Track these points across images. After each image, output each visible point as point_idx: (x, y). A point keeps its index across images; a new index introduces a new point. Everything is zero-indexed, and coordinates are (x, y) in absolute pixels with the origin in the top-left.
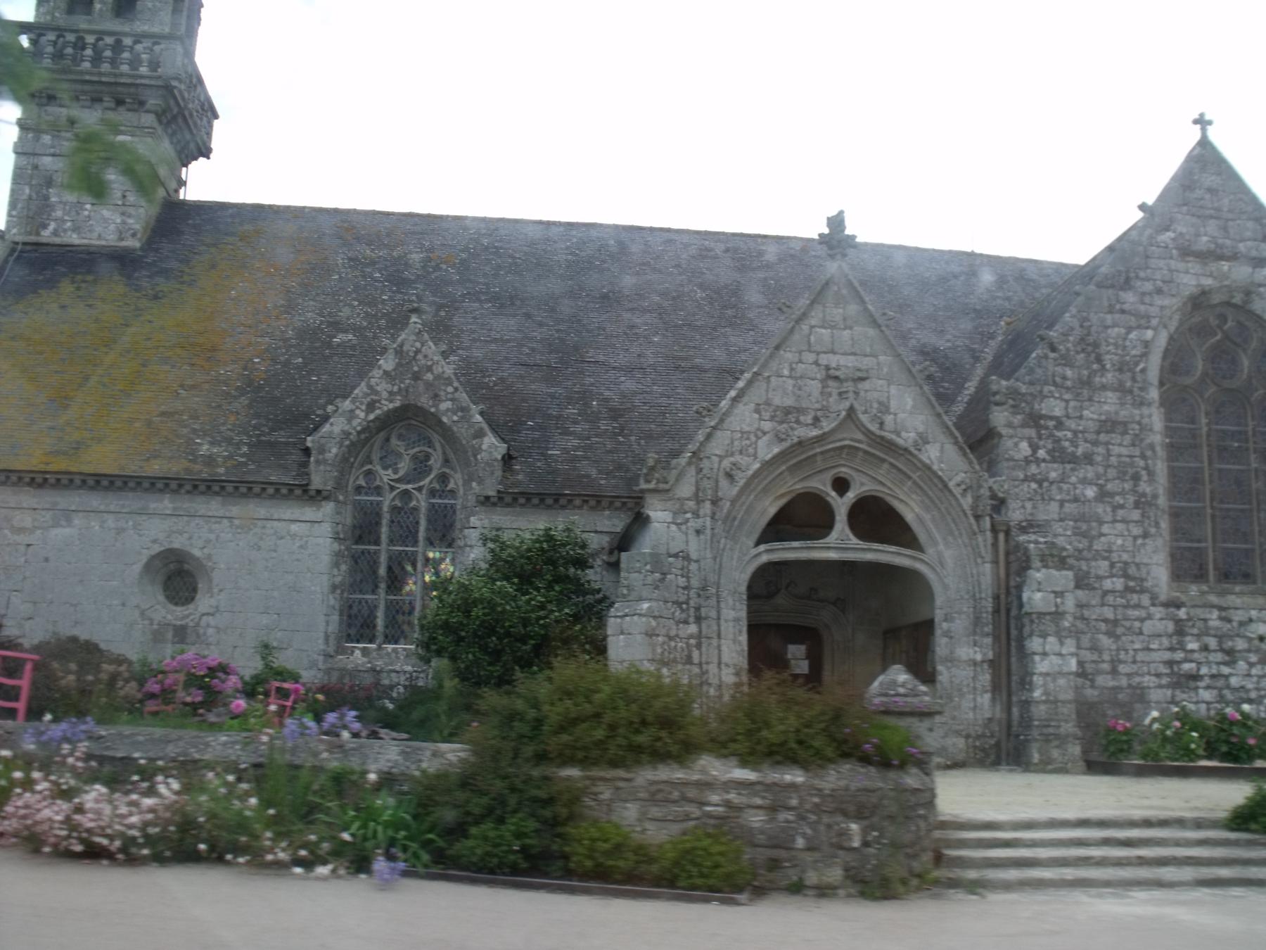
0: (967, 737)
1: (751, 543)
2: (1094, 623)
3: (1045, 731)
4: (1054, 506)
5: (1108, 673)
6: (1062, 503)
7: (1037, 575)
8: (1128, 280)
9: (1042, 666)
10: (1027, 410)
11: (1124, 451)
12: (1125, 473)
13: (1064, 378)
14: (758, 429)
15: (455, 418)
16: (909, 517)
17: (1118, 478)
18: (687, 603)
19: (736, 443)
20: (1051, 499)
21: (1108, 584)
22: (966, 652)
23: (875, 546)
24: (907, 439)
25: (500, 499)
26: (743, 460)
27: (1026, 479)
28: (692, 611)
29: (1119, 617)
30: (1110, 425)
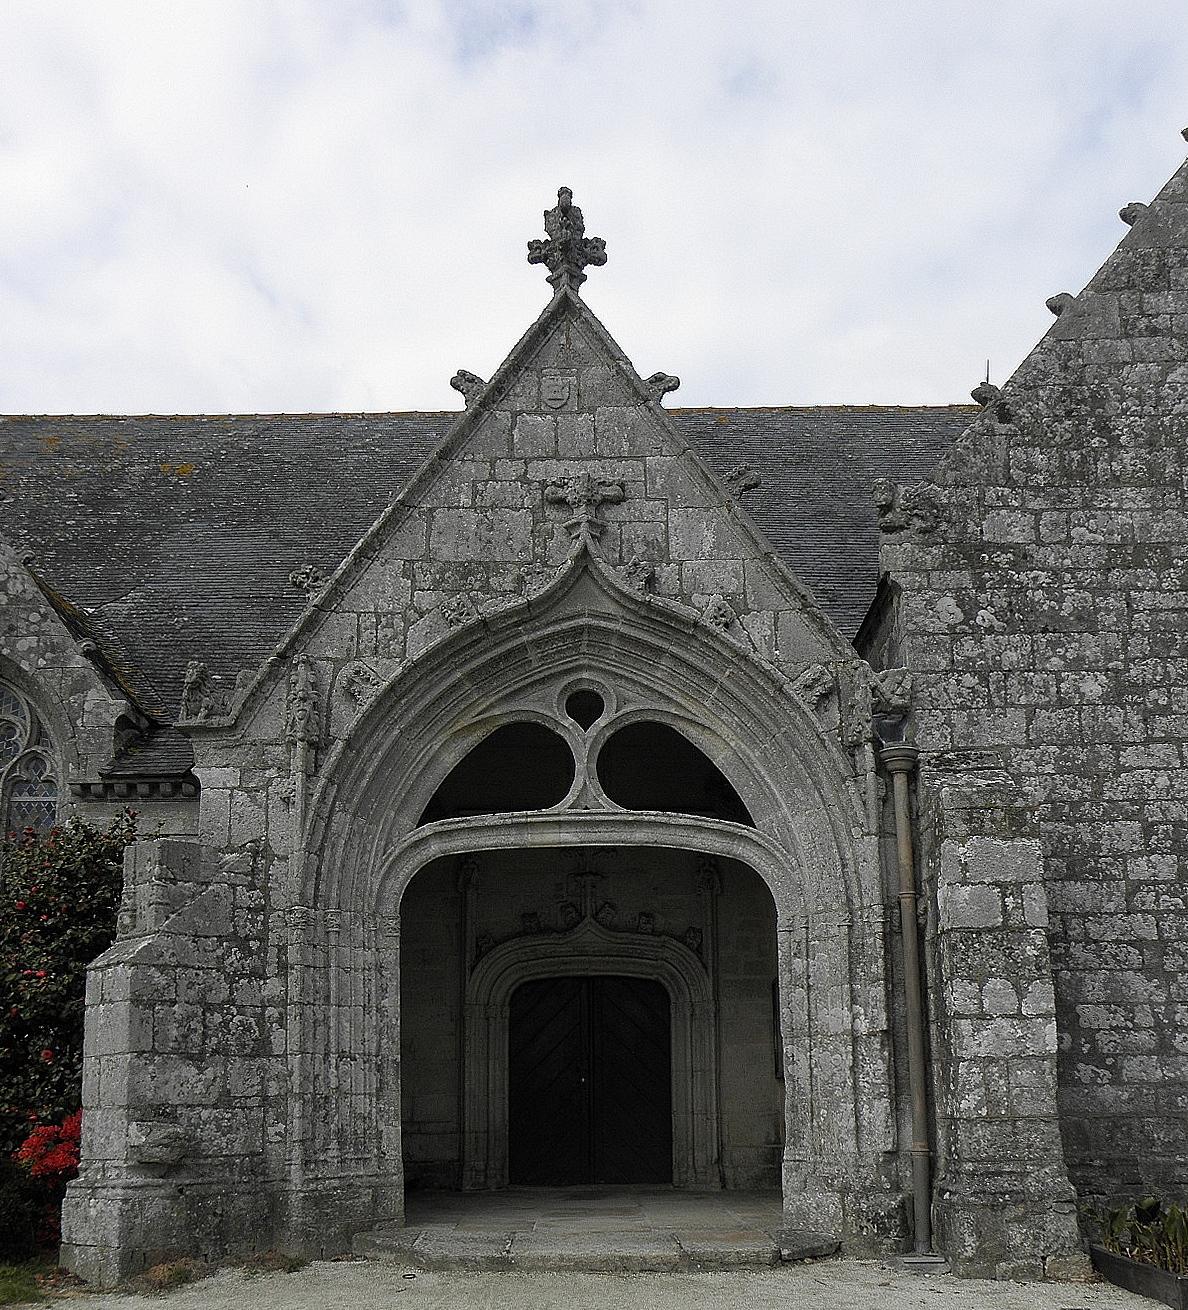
0: (844, 1191)
1: (407, 820)
2: (1112, 949)
3: (990, 1185)
4: (1015, 719)
5: (1150, 1053)
6: (1031, 712)
7: (958, 851)
8: (1162, 271)
9: (975, 1042)
10: (952, 535)
11: (1165, 601)
12: (1169, 644)
13: (1030, 469)
14: (410, 607)
15: (42, 662)
16: (720, 759)
17: (1154, 654)
18: (262, 939)
19: (365, 635)
20: (1007, 704)
21: (1140, 868)
22: (835, 1016)
23: (652, 815)
24: (704, 606)
25: (108, 788)
26: (368, 663)
27: (953, 668)
28: (273, 952)
29: (1172, 935)
30: (1131, 553)
